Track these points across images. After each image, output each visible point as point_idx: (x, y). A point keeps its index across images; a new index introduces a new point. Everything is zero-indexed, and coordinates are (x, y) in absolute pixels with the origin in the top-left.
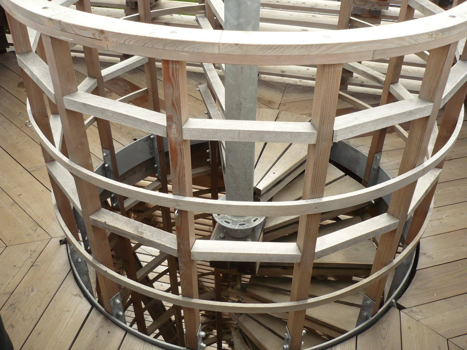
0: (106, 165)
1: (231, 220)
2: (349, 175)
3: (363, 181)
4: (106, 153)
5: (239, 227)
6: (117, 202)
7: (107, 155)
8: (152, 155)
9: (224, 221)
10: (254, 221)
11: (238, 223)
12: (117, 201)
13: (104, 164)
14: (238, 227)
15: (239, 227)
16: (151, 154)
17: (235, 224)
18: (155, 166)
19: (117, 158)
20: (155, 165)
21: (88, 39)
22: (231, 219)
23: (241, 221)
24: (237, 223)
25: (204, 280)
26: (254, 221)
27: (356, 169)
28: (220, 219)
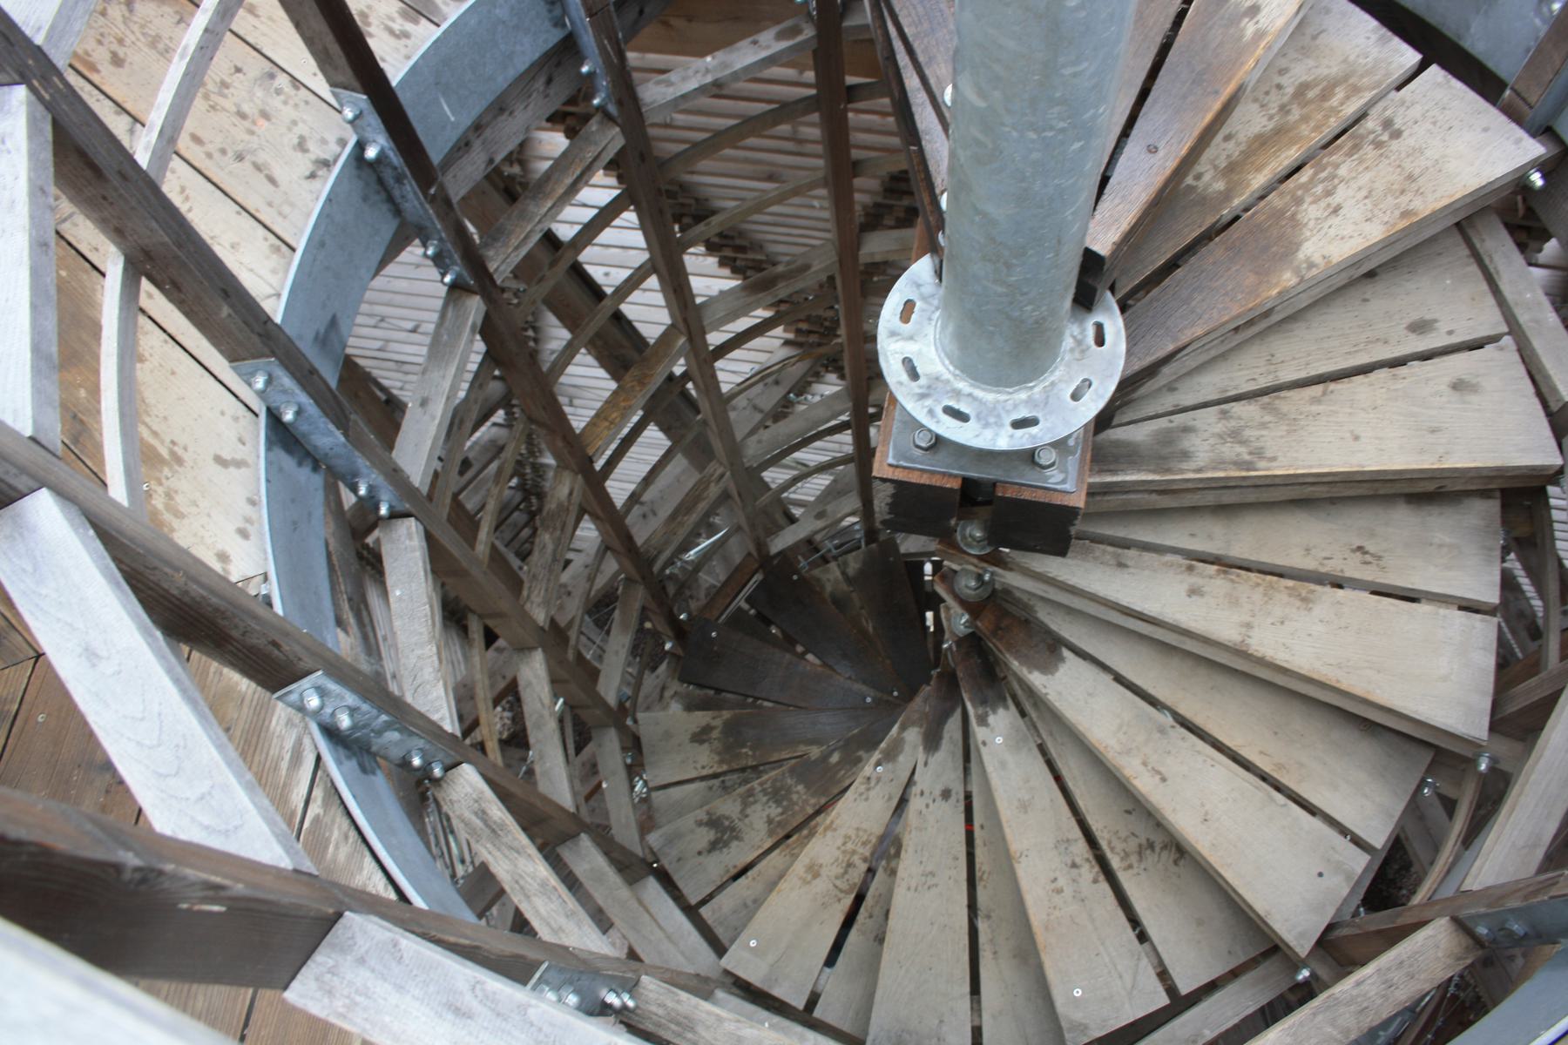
0: (371, 153)
1: (970, 399)
2: (1444, 66)
3: (1508, 92)
4: (354, 104)
5: (1012, 436)
6: (457, 268)
7: (361, 113)
8: (564, 25)
9: (939, 410)
10: (1076, 396)
11: (1004, 415)
12: (454, 263)
13: (360, 146)
14: (1007, 439)
15: (1012, 436)
16: (558, 23)
17: (992, 420)
18: (585, 69)
19: (405, 98)
20: (581, 65)
21: (244, 1000)
22: (970, 395)
23: (1015, 406)
24: (999, 416)
25: (905, 66)
26: (1076, 396)
27: (1468, 28)
28: (923, 396)
